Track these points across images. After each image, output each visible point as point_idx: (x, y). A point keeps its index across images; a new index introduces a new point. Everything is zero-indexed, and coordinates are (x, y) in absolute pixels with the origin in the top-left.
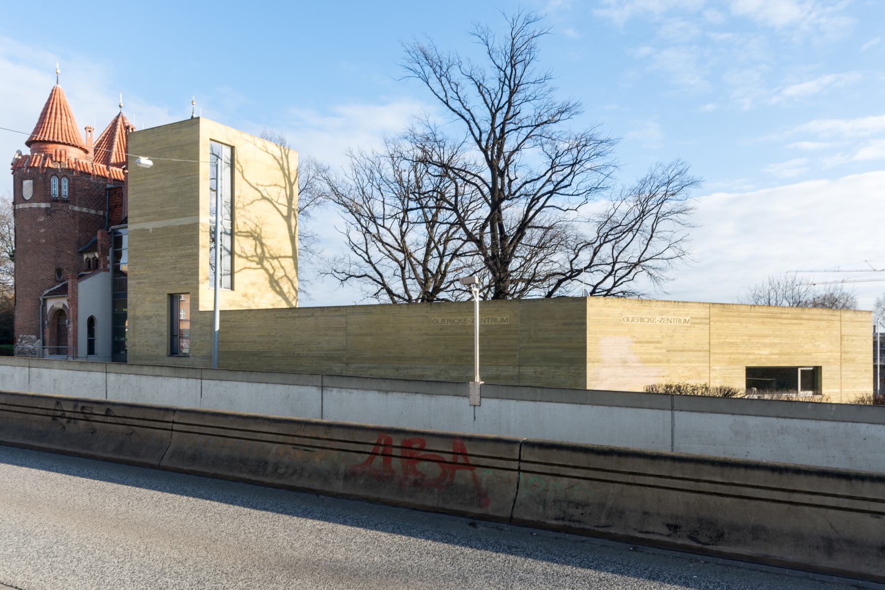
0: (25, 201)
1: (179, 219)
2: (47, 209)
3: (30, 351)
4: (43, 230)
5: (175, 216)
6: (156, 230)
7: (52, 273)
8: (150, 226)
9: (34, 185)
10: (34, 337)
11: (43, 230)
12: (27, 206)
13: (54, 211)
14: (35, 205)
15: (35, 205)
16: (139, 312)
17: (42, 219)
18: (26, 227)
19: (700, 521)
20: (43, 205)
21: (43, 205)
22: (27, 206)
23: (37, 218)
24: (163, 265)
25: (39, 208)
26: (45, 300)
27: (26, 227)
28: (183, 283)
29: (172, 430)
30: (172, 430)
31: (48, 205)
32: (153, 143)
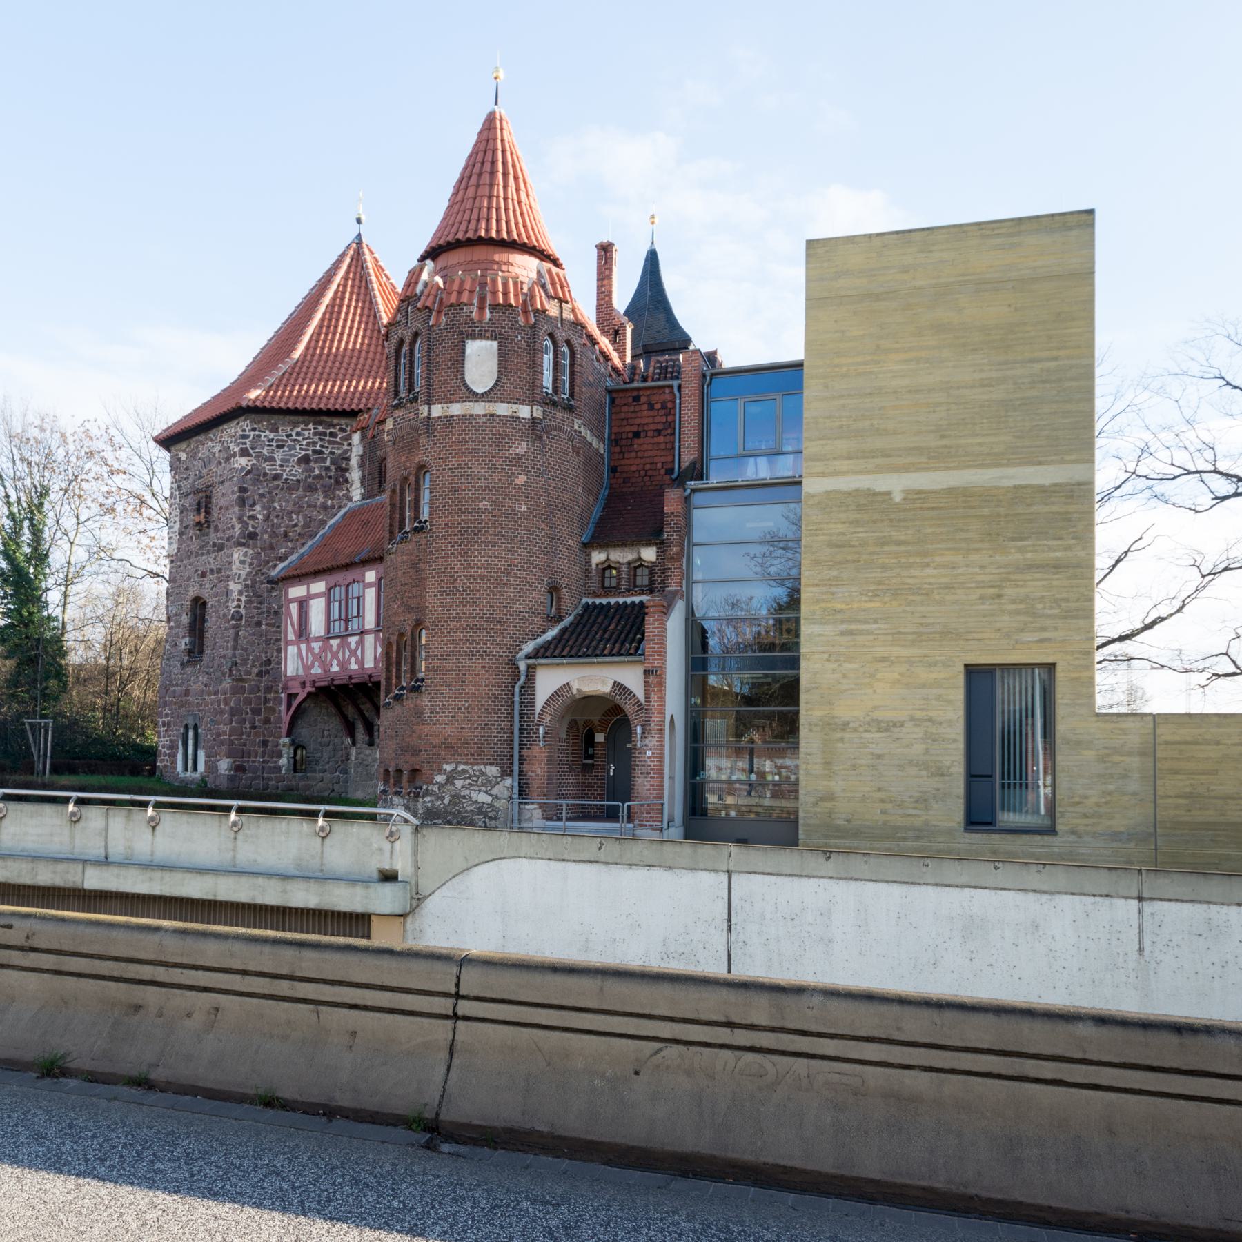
0: (475, 397)
1: (1011, 471)
2: (534, 421)
3: (481, 809)
4: (522, 479)
5: (996, 460)
6: (916, 497)
7: (539, 596)
8: (896, 484)
9: (503, 356)
10: (493, 770)
11: (522, 479)
12: (478, 409)
13: (547, 431)
14: (502, 409)
15: (502, 409)
16: (845, 710)
17: (520, 448)
18: (476, 468)
19: (116, 1182)
20: (524, 412)
21: (524, 412)
22: (478, 409)
23: (510, 444)
24: (947, 587)
25: (515, 419)
26: (531, 670)
27: (476, 468)
28: (1028, 637)
29: (455, 1017)
30: (455, 1017)
31: (538, 412)
32: (905, 269)
